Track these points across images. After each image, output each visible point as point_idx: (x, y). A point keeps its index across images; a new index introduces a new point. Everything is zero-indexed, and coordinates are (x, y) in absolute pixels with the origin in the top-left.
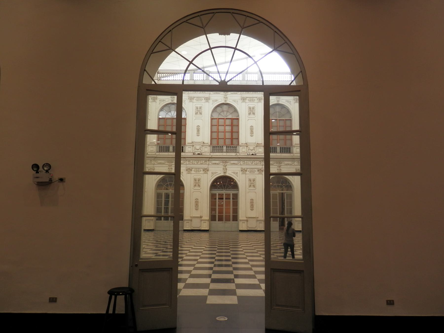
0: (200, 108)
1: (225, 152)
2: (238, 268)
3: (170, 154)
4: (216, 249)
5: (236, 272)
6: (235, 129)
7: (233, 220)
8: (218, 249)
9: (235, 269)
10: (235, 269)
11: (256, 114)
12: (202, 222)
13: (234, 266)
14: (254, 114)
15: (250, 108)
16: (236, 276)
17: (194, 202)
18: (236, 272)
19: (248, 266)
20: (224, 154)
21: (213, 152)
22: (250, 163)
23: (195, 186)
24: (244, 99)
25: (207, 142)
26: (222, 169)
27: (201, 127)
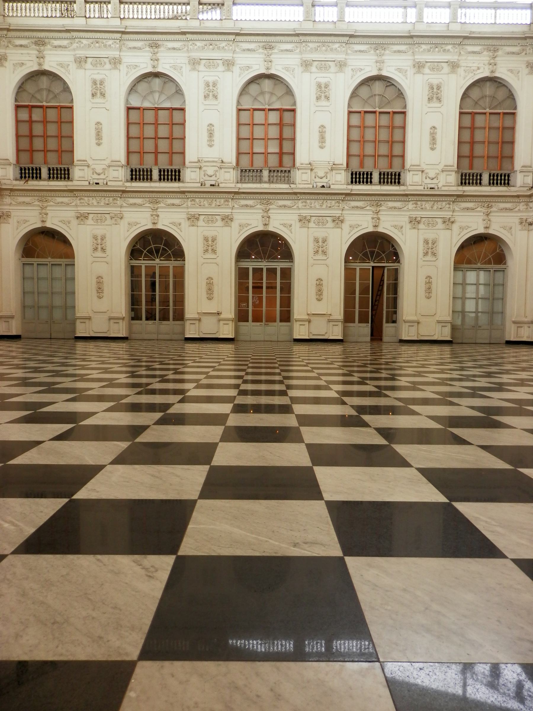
21: (241, 180)
24: (306, 65)
25: (230, 161)
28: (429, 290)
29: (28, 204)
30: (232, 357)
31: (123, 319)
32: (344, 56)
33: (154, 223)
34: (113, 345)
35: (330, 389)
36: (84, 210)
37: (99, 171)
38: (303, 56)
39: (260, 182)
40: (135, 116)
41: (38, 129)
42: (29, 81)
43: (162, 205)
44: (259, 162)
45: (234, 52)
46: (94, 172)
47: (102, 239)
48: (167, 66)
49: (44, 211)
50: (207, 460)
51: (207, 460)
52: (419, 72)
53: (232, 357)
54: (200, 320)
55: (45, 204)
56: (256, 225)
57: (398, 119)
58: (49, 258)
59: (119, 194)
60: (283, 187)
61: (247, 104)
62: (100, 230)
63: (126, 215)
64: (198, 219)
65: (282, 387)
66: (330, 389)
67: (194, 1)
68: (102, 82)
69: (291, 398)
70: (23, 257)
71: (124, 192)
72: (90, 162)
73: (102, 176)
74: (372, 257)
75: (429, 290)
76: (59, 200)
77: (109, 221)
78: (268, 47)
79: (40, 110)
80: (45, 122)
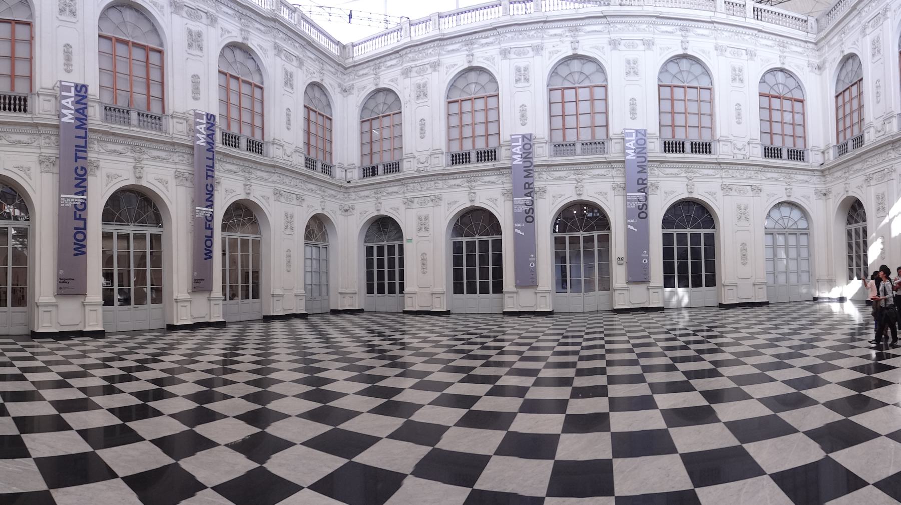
0: (526, 69)
1: (135, 126)
2: (503, 362)
3: (470, 165)
4: (583, 334)
5: (609, 357)
6: (21, 50)
7: (154, 301)
8: (587, 334)
9: (609, 351)
10: (609, 351)
11: (79, 13)
12: (538, 295)
13: (607, 347)
14: (527, 80)
15: (518, 69)
16: (610, 363)
17: (739, 250)
18: (609, 357)
19: (623, 332)
20: (134, 131)
21: (556, 154)
22: (737, 174)
23: (420, 230)
24: (505, 53)
25: (542, 136)
26: (130, 167)
27: (75, 50)
28: (744, 257)
29: (564, 178)
30: (551, 335)
31: (549, 292)
32: (540, 41)
33: (471, 201)
34: (540, 319)
35: (13, 366)
36: (410, 195)
37: (422, 160)
38: (502, 45)
39: (575, 154)
40: (455, 108)
41: (570, 108)
42: (561, 66)
43: (479, 183)
44: (571, 136)
45: (439, 54)
46: (419, 162)
47: (426, 220)
48: (481, 59)
49: (579, 184)
50: (551, 455)
51: (551, 455)
52: (505, 58)
53: (551, 335)
54: (56, 306)
55: (473, 184)
56: (463, 202)
57: (492, 102)
58: (477, 236)
59: (544, 168)
60: (599, 157)
61: (558, 83)
62: (423, 212)
63: (445, 196)
64: (412, 202)
65: (636, 370)
66: (13, 366)
67: (505, 2)
68: (425, 85)
69: (651, 385)
70: (452, 236)
71: (548, 165)
72: (416, 154)
73: (426, 164)
74: (688, 223)
75: (744, 257)
76: (487, 179)
77: (431, 204)
78: (576, 29)
79: (469, 102)
80: (473, 111)
